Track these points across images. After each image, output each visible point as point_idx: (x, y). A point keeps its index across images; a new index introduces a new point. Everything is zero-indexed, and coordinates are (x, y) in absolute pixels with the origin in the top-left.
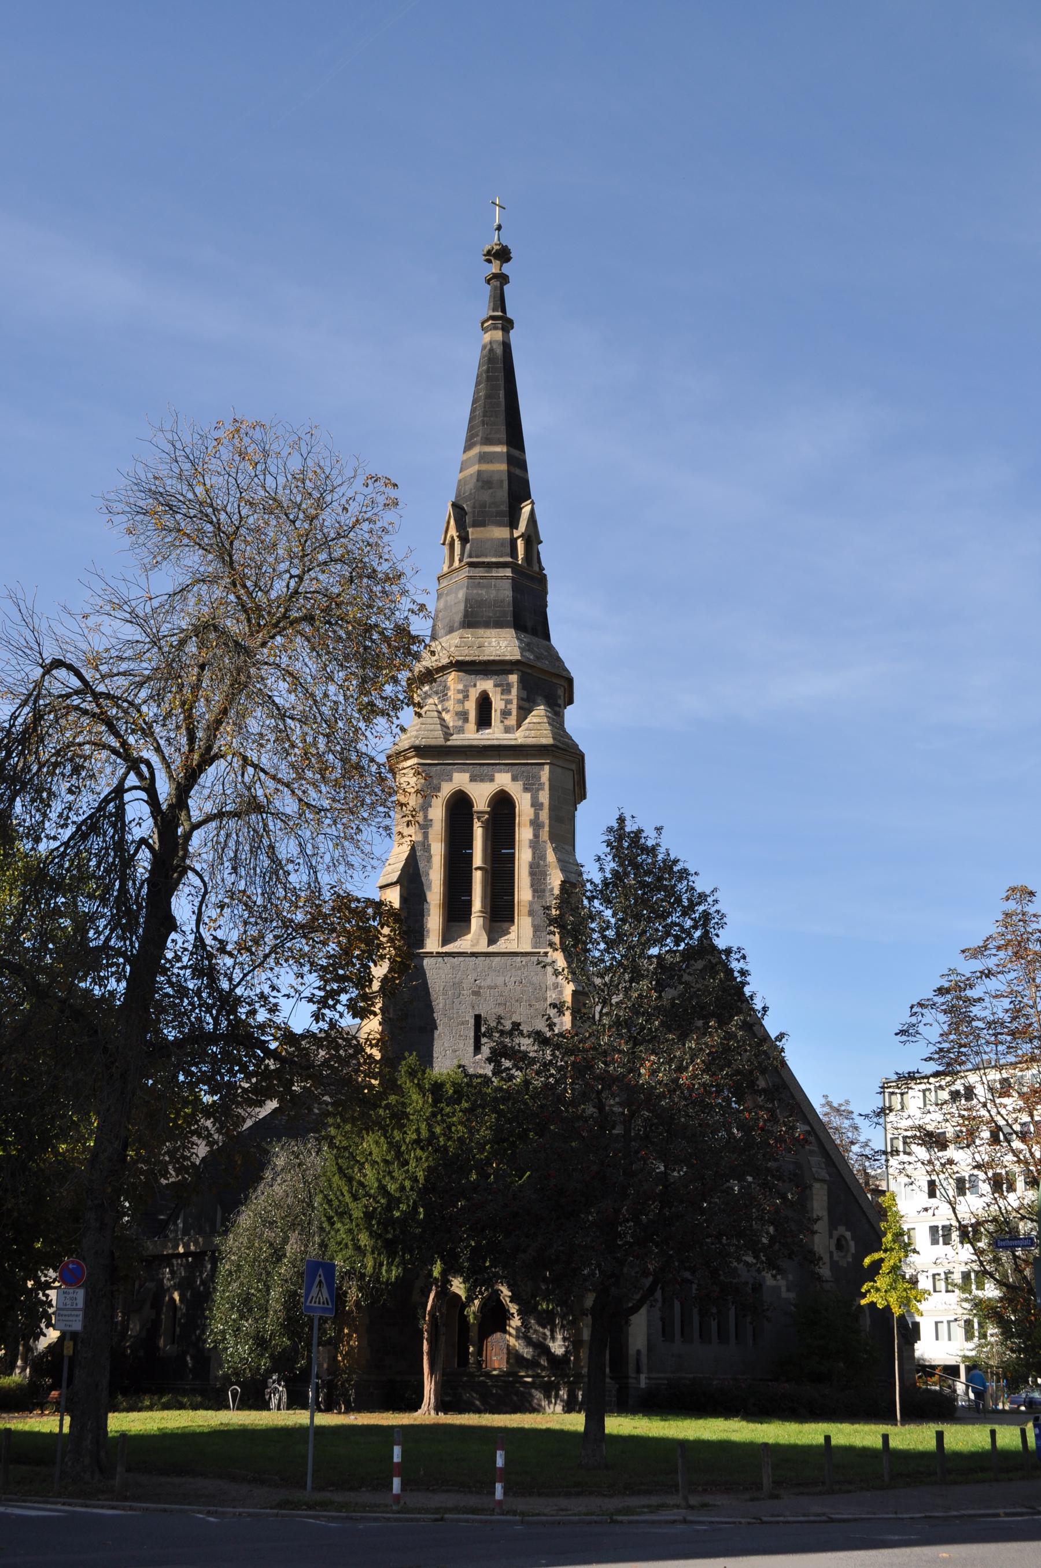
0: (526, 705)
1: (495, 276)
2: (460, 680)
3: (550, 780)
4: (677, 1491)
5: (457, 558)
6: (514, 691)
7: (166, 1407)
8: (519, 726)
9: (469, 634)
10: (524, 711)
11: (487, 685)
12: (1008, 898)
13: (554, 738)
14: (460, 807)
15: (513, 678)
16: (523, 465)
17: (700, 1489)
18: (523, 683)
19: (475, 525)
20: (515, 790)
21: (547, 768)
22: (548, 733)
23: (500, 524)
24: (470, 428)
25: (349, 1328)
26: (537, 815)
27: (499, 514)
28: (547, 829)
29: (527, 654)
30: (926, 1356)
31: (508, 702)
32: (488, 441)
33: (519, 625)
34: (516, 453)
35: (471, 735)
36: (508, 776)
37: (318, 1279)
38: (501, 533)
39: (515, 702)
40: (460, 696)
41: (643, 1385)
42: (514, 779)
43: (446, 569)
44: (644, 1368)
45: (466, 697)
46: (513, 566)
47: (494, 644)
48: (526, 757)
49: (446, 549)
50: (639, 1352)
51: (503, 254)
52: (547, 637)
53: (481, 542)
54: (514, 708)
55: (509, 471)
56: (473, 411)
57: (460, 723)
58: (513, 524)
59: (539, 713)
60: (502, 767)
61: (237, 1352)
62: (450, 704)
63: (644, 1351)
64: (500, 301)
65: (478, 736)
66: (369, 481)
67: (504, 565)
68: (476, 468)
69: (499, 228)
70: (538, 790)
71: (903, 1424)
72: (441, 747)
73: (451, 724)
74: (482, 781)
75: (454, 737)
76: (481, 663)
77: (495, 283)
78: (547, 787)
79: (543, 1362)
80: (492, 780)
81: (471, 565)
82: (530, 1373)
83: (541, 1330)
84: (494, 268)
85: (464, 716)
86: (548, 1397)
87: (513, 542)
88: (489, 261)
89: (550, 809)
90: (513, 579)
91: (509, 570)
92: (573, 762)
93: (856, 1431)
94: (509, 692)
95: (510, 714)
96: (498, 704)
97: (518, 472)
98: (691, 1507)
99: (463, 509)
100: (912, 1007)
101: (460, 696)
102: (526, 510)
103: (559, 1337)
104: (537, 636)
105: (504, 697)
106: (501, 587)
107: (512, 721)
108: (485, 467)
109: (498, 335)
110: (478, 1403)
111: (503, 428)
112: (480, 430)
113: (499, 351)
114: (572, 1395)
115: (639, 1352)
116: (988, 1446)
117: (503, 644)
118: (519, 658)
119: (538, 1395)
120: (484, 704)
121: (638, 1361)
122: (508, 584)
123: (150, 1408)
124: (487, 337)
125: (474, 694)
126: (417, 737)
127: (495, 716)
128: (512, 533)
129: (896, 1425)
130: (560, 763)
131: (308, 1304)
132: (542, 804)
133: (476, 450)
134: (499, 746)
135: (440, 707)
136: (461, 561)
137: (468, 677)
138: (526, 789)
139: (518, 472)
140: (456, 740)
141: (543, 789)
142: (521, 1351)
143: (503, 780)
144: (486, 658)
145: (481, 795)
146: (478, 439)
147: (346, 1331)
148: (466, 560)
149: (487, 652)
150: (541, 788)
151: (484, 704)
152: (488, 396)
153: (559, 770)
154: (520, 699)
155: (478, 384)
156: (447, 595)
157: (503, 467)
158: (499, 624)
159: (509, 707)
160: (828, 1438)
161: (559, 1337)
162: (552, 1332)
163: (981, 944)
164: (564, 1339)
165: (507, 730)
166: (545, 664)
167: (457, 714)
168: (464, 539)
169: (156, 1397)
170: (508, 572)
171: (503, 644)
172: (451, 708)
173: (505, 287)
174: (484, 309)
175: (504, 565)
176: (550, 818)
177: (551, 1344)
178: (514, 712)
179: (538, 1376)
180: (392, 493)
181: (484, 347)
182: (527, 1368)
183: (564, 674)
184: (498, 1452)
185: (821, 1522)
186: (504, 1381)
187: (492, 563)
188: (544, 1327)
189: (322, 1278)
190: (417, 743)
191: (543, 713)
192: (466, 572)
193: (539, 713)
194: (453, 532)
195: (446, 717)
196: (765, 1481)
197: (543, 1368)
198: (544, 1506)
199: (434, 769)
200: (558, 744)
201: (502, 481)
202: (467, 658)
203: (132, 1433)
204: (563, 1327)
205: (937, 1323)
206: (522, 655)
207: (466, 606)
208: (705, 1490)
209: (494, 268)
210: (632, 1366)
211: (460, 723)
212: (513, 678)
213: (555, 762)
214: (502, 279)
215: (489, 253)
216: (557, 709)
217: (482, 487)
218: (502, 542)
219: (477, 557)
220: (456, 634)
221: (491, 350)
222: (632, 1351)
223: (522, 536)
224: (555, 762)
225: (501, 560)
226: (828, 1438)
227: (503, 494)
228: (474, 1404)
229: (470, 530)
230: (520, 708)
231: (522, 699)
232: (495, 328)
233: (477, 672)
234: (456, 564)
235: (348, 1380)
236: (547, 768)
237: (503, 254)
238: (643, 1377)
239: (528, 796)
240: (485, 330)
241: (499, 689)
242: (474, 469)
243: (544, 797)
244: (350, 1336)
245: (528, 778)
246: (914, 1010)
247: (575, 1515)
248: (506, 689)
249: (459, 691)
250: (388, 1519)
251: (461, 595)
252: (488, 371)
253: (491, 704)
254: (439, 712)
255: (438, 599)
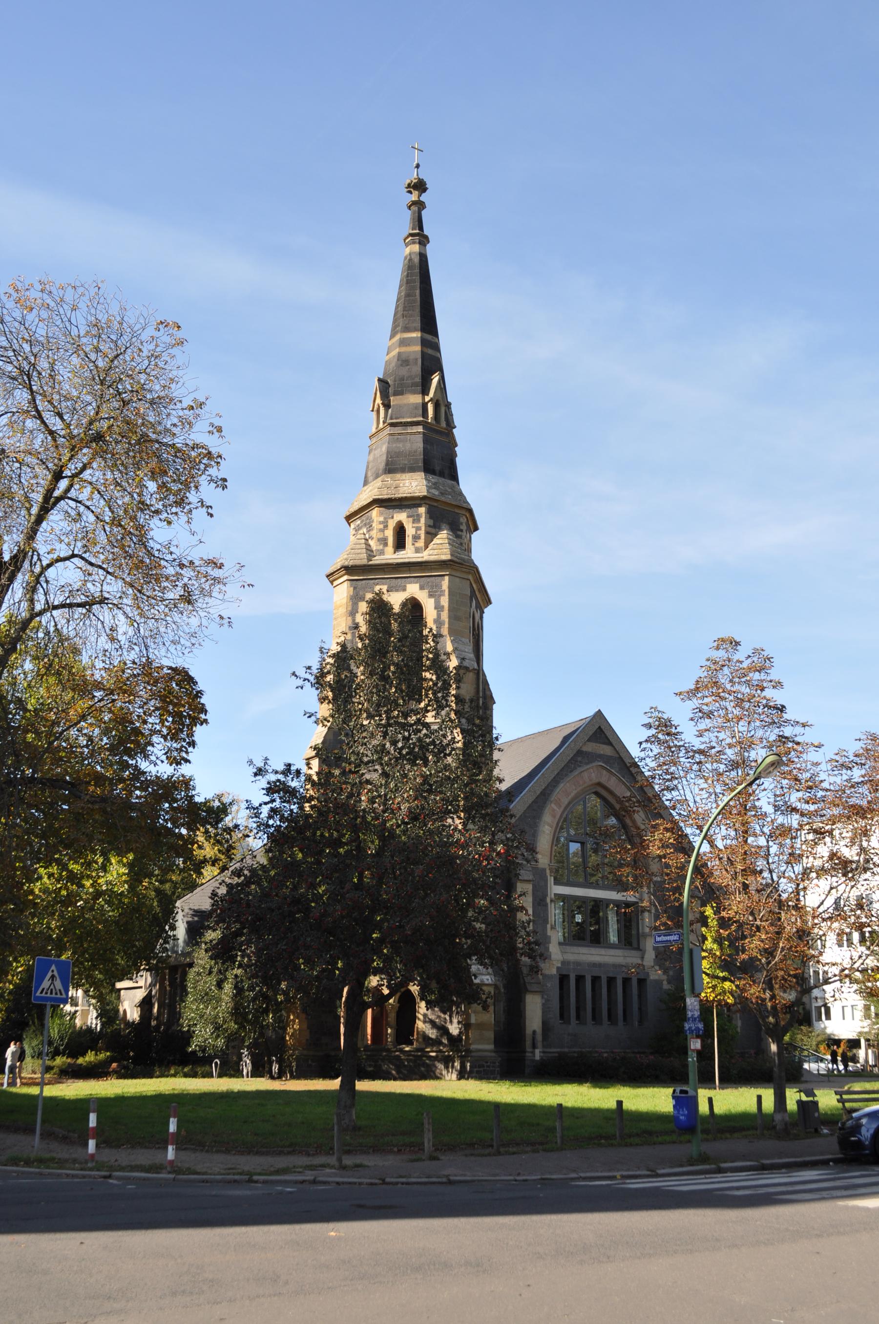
0: (433, 531)
1: (414, 203)
2: (381, 514)
3: (449, 588)
4: (333, 1154)
5: (381, 421)
6: (423, 520)
7: (186, 1075)
8: (426, 547)
9: (388, 478)
10: (431, 535)
11: (402, 516)
12: (718, 648)
13: (452, 555)
14: (379, 607)
15: (422, 510)
16: (436, 347)
17: (396, 1149)
18: (430, 513)
19: (396, 394)
20: (422, 597)
21: (447, 578)
22: (448, 551)
23: (414, 393)
24: (395, 321)
25: (294, 1015)
26: (439, 616)
27: (414, 385)
28: (447, 625)
29: (433, 491)
30: (835, 1033)
31: (418, 529)
32: (407, 329)
33: (428, 469)
34: (429, 337)
35: (390, 556)
36: (417, 586)
37: (50, 974)
38: (416, 399)
39: (423, 528)
40: (381, 526)
41: (537, 1057)
42: (422, 588)
43: (374, 430)
44: (539, 1044)
45: (386, 527)
46: (425, 424)
47: (407, 485)
48: (431, 570)
49: (374, 414)
50: (534, 1032)
51: (420, 186)
52: (454, 477)
53: (400, 406)
54: (422, 533)
55: (422, 352)
56: (397, 308)
57: (381, 547)
58: (425, 391)
59: (443, 536)
60: (412, 579)
61: (203, 1036)
62: (374, 533)
63: (539, 1031)
64: (419, 223)
65: (395, 556)
66: (160, 326)
67: (417, 424)
68: (397, 350)
69: (418, 166)
70: (440, 596)
71: (721, 1088)
72: (365, 566)
73: (374, 549)
74: (397, 591)
75: (376, 558)
76: (395, 500)
77: (415, 208)
78: (447, 593)
79: (445, 1041)
80: (404, 590)
81: (392, 425)
82: (434, 1049)
83: (443, 1015)
84: (414, 197)
85: (384, 541)
86: (447, 1067)
87: (424, 406)
88: (410, 192)
89: (449, 610)
90: (424, 434)
91: (421, 427)
92: (469, 573)
93: (637, 1096)
94: (419, 521)
95: (419, 538)
96: (410, 531)
97: (430, 351)
98: (344, 1168)
99: (387, 383)
100: (641, 743)
101: (381, 526)
102: (435, 379)
103: (455, 1021)
104: (444, 477)
105: (415, 525)
106: (414, 441)
107: (421, 543)
108: (404, 349)
109: (416, 248)
110: (394, 1072)
111: (418, 318)
112: (401, 322)
113: (416, 260)
114: (463, 1066)
115: (534, 1032)
116: (754, 1108)
117: (414, 484)
118: (426, 494)
119: (441, 1066)
120: (400, 531)
121: (534, 1039)
122: (420, 438)
123: (174, 1076)
124: (408, 250)
125: (392, 524)
126: (346, 559)
127: (409, 541)
128: (424, 399)
129: (715, 1088)
130: (458, 574)
131: (38, 994)
132: (443, 607)
133: (397, 337)
134: (409, 563)
135: (367, 536)
136: (384, 422)
137: (388, 511)
138: (430, 596)
139: (430, 351)
140: (377, 560)
141: (444, 595)
142: (427, 1032)
143: (413, 589)
144: (400, 496)
145: (396, 600)
146: (399, 328)
147: (292, 1017)
148: (389, 421)
149: (401, 491)
150: (442, 593)
151: (400, 531)
152: (408, 295)
153: (458, 580)
154: (427, 526)
155: (400, 287)
156: (375, 449)
157: (418, 348)
158: (412, 469)
159: (419, 532)
160: (620, 1103)
161: (455, 1021)
162: (451, 1017)
163: (693, 687)
164: (459, 1023)
165: (417, 550)
166: (448, 499)
167: (379, 540)
168: (387, 406)
169: (180, 1068)
170: (420, 429)
171: (414, 484)
172: (374, 536)
173: (423, 212)
174: (406, 226)
175: (417, 424)
176: (450, 617)
177: (450, 1027)
178: (423, 536)
179: (440, 1051)
180: (180, 334)
181: (406, 258)
182: (432, 1045)
183: (465, 505)
184: (171, 1120)
185: (439, 1183)
186: (413, 1056)
187: (408, 422)
188: (445, 1013)
189: (55, 973)
190: (346, 564)
191: (445, 536)
192: (388, 430)
193: (443, 536)
194: (379, 401)
195: (371, 542)
196: (426, 1144)
197: (445, 1046)
198: (214, 1164)
199: (360, 583)
200: (455, 559)
201: (417, 359)
202: (386, 497)
203: (588, 1084)
204: (458, 1013)
205: (843, 1007)
206: (428, 491)
207: (387, 457)
208: (399, 1151)
209: (414, 197)
210: (528, 1043)
211: (381, 547)
212: (422, 510)
213: (454, 573)
214: (419, 205)
215: (409, 186)
216: (460, 533)
217: (401, 365)
218: (415, 406)
219: (396, 418)
220: (380, 479)
221: (410, 260)
222: (529, 1031)
223: (431, 400)
224: (454, 573)
225: (415, 419)
226: (620, 1103)
227: (417, 369)
228: (390, 1073)
229: (392, 398)
230: (427, 533)
231: (430, 526)
232: (414, 243)
233: (394, 507)
234: (381, 426)
235: (292, 1055)
236: (447, 578)
237: (420, 186)
238: (537, 1051)
239: (432, 601)
240: (407, 245)
241: (411, 519)
242: (395, 353)
243: (445, 601)
244: (294, 1021)
245: (432, 587)
246: (643, 746)
247: (241, 1174)
248: (416, 519)
249: (380, 523)
250: (73, 1176)
251: (384, 448)
252: (407, 276)
253: (405, 531)
254: (367, 540)
255: (370, 453)
